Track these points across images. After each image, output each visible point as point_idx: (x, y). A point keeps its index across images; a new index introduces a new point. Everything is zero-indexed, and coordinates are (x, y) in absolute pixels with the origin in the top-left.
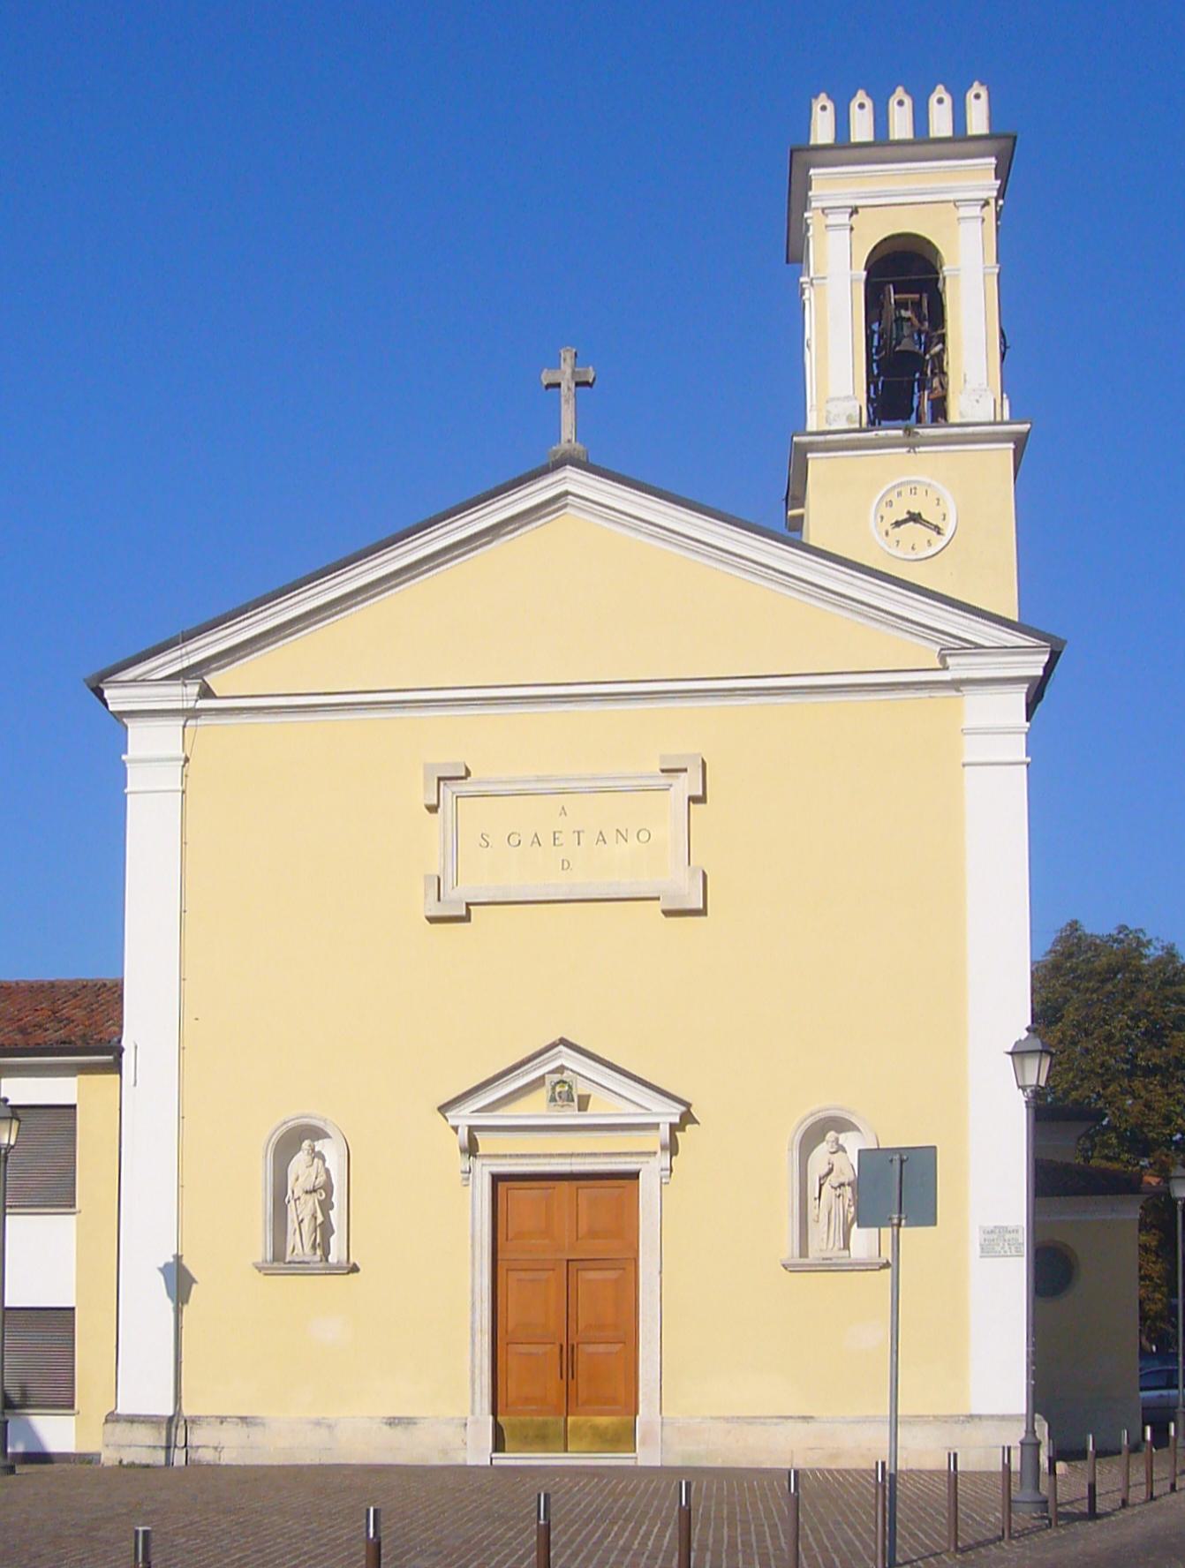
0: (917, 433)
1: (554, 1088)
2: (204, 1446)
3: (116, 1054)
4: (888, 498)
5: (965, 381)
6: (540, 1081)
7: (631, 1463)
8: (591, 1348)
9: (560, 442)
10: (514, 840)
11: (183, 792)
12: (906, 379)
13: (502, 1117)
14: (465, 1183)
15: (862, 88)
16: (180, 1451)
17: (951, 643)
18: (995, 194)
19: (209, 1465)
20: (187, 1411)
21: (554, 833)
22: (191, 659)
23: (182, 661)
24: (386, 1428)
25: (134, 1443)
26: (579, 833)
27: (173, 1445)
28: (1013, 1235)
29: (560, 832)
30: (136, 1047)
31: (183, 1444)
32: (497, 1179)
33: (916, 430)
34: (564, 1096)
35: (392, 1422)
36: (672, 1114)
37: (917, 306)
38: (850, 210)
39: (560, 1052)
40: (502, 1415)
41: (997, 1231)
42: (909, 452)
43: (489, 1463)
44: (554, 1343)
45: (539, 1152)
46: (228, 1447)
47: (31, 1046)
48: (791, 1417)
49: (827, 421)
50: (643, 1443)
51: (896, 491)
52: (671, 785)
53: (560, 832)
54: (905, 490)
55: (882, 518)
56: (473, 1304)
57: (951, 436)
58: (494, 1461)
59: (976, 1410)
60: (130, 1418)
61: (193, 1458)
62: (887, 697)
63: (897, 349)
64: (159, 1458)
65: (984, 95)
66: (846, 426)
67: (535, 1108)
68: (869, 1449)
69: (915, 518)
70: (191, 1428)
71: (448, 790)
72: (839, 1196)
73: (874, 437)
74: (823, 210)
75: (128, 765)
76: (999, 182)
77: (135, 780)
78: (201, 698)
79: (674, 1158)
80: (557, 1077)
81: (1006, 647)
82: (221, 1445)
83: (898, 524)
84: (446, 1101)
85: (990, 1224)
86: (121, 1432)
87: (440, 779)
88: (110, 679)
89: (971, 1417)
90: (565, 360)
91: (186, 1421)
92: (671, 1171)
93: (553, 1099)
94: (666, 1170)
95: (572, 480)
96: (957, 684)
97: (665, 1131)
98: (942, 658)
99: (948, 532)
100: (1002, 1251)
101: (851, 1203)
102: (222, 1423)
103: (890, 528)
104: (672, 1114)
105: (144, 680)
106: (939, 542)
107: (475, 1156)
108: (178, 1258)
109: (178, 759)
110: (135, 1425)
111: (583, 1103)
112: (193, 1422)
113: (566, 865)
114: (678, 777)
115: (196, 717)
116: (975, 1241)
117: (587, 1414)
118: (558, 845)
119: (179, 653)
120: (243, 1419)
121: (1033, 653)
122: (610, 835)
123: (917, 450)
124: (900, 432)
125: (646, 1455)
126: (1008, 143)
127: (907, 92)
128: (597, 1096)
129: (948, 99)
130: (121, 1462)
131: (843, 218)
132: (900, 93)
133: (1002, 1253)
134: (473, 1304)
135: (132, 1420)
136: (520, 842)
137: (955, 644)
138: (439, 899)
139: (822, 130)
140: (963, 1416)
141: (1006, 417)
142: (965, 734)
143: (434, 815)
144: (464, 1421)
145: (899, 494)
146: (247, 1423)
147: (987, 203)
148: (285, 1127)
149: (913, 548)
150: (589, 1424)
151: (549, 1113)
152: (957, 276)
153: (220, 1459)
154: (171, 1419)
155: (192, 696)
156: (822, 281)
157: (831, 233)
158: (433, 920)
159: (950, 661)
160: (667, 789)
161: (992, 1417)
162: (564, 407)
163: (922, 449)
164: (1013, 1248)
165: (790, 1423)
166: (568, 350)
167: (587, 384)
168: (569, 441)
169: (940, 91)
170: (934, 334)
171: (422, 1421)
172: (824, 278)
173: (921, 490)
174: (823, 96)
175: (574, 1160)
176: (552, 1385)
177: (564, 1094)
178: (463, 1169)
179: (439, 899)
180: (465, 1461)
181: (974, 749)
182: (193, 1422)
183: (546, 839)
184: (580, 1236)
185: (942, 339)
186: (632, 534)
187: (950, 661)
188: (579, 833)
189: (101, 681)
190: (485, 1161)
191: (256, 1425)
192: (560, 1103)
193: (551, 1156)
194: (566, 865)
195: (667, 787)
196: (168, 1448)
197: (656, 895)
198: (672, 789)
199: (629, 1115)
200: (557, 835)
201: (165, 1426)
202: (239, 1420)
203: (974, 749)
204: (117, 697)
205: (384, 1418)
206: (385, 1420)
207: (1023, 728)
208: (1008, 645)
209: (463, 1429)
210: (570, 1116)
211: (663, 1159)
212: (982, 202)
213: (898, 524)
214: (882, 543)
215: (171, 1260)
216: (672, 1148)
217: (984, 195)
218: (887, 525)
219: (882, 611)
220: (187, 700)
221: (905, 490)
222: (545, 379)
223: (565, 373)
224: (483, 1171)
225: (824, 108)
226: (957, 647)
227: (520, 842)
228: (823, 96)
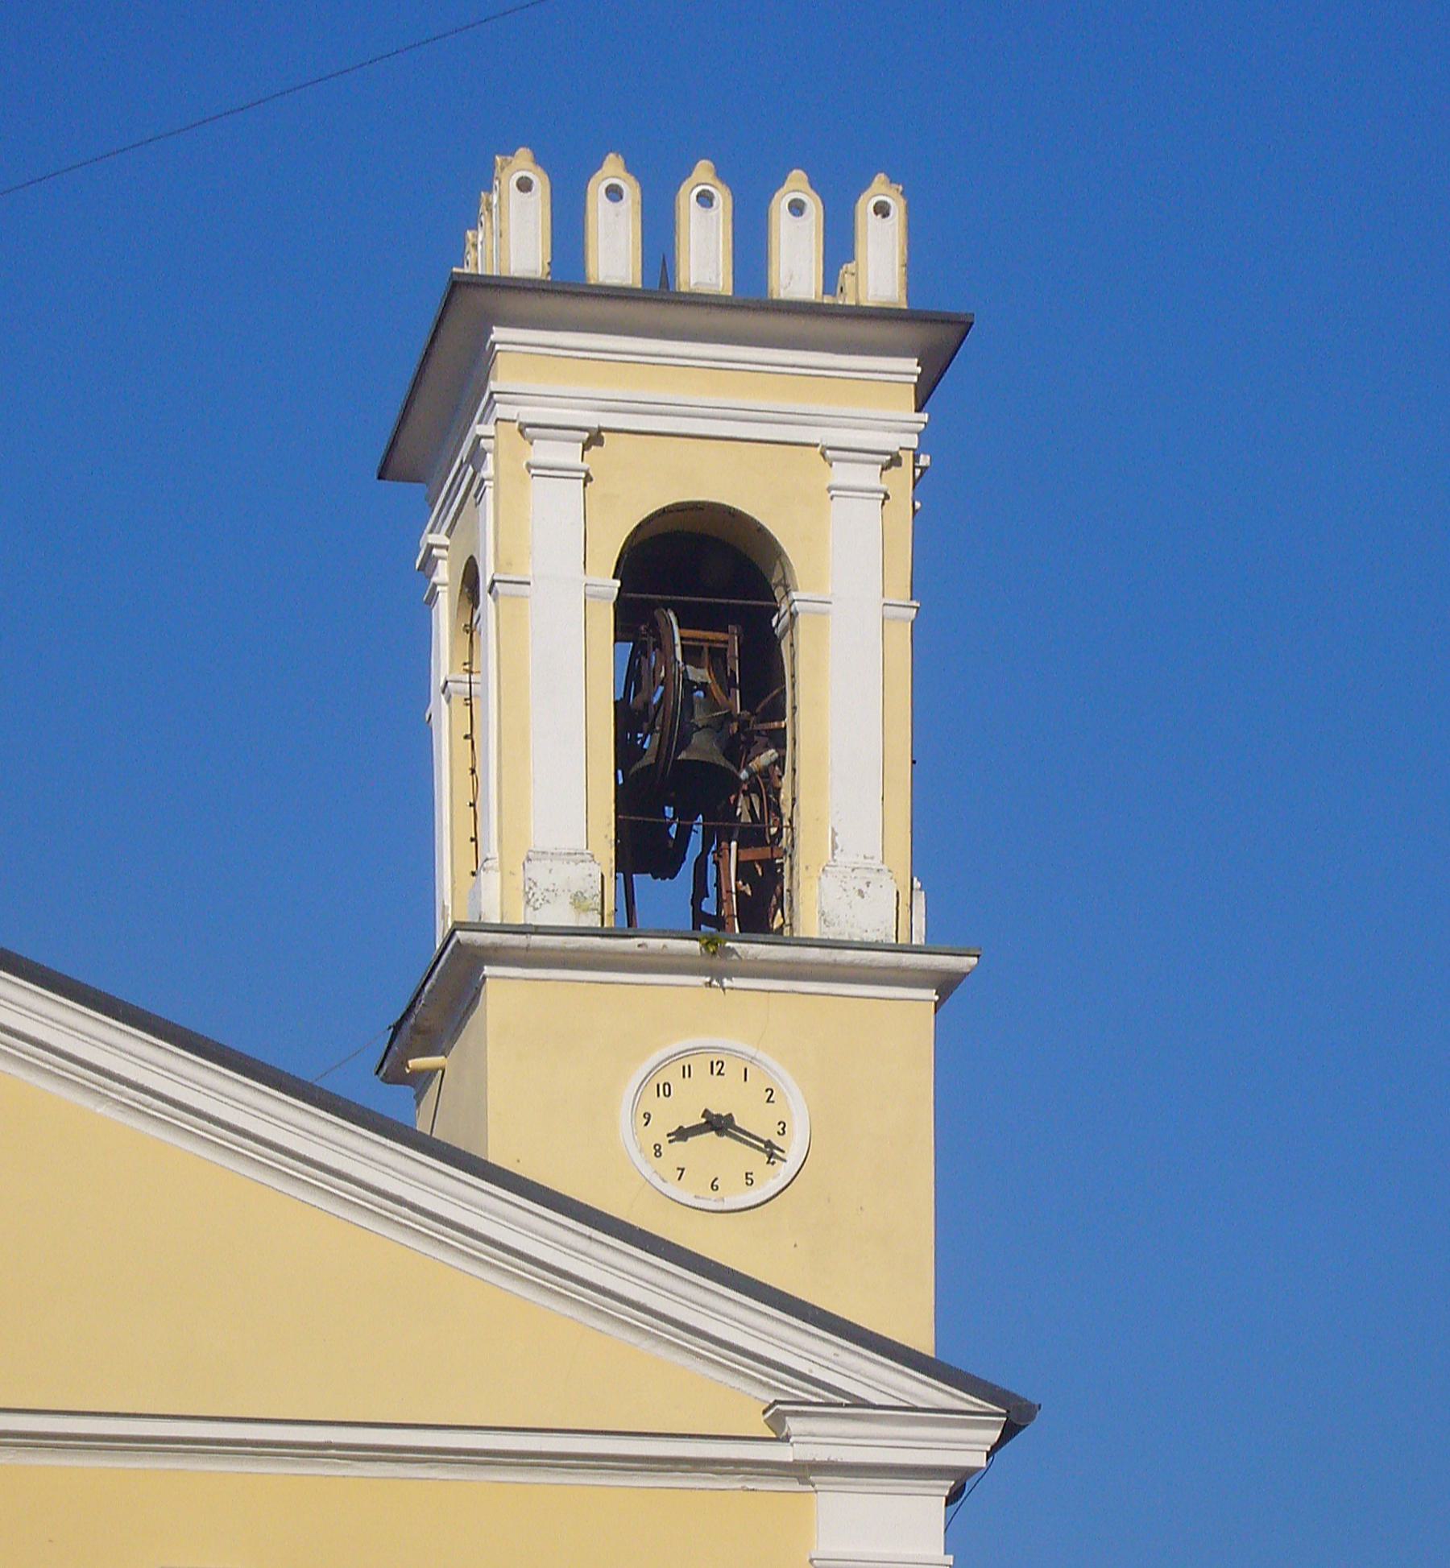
0: (732, 951)
5: (834, 847)
15: (618, 152)
18: (913, 441)
37: (718, 656)
44: (883, 862)
51: (679, 1065)
63: (683, 756)
65: (897, 207)
66: (569, 919)
69: (718, 1124)
83: (682, 1134)
98: (776, 1419)
99: (794, 1148)
103: (664, 1141)
106: (772, 1179)
127: (721, 174)
129: (814, 207)
131: (569, 454)
132: (703, 174)
137: (819, 1396)
141: (918, 940)
145: (687, 1072)
147: (895, 461)
152: (825, 613)
159: (793, 1425)
170: (760, 727)
173: (733, 1069)
174: (524, 156)
185: (778, 739)
186: (87, 1102)
187: (793, 1425)
208: (920, 1405)
213: (682, 1134)
214: (647, 1171)
217: (892, 442)
221: (700, 1065)
226: (815, 1399)
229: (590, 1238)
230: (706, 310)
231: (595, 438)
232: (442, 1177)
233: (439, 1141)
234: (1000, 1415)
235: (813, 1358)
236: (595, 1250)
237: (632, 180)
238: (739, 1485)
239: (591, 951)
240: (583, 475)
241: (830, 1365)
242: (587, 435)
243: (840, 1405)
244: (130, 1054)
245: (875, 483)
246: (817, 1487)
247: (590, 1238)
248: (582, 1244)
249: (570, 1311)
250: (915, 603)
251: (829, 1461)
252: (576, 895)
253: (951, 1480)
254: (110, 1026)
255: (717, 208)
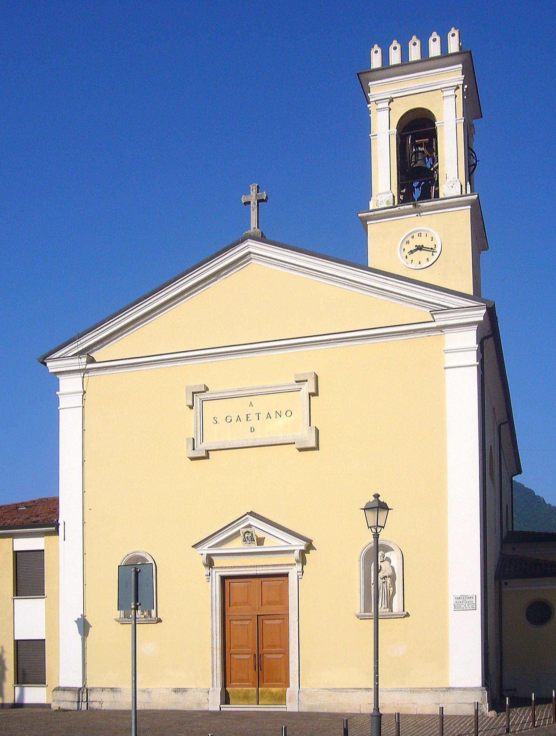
0: (420, 206)
1: (244, 535)
2: (95, 701)
3: (56, 526)
4: (407, 240)
5: (446, 178)
6: (237, 534)
7: (284, 710)
8: (268, 656)
9: (250, 229)
10: (228, 419)
11: (83, 407)
12: (410, 182)
13: (223, 549)
14: (208, 580)
15: (395, 39)
16: (84, 703)
17: (437, 308)
18: (462, 82)
19: (97, 710)
20: (89, 686)
21: (247, 415)
22: (79, 349)
23: (78, 348)
24: (173, 693)
25: (65, 700)
26: (258, 414)
27: (81, 700)
28: (471, 600)
29: (250, 414)
30: (64, 523)
31: (86, 700)
32: (223, 579)
33: (418, 204)
34: (250, 539)
35: (176, 690)
36: (301, 545)
38: (388, 100)
39: (248, 518)
40: (228, 687)
41: (462, 598)
42: (417, 216)
43: (219, 710)
45: (241, 565)
46: (105, 702)
47: (21, 524)
48: (361, 689)
49: (377, 205)
50: (290, 701)
52: (301, 388)
53: (250, 414)
54: (416, 235)
55: (404, 249)
56: (212, 636)
57: (437, 205)
58: (221, 708)
59: (451, 685)
60: (64, 689)
61: (90, 706)
62: (205, 361)
64: (75, 706)
67: (237, 545)
68: (398, 704)
69: (420, 248)
70: (89, 693)
71: (197, 398)
72: (384, 582)
73: (398, 210)
74: (375, 101)
75: (59, 397)
76: (464, 76)
77: (63, 402)
78: (88, 364)
79: (304, 566)
80: (245, 530)
81: (463, 308)
82: (102, 701)
83: (412, 252)
84: (196, 543)
85: (459, 595)
86: (60, 695)
87: (193, 393)
88: (48, 358)
89: (449, 688)
90: (252, 190)
91: (87, 690)
92: (303, 573)
93: (245, 541)
94: (300, 572)
95: (252, 246)
96: (440, 328)
97: (297, 553)
99: (438, 249)
100: (465, 608)
101: (391, 586)
102: (103, 691)
103: (408, 255)
104: (301, 545)
105: (64, 357)
107: (212, 568)
108: (83, 616)
109: (80, 392)
110: (66, 692)
111: (260, 542)
112: (91, 690)
113: (252, 430)
114: (304, 384)
115: (88, 373)
116: (451, 602)
117: (267, 686)
118: (249, 421)
119: (76, 344)
120: (112, 689)
121: (466, 311)
122: (273, 414)
123: (421, 214)
124: (411, 206)
125: (291, 707)
126: (466, 56)
128: (268, 538)
130: (59, 708)
133: (465, 609)
134: (212, 636)
135: (64, 689)
136: (231, 420)
137: (438, 308)
138: (194, 449)
139: (376, 61)
140: (445, 688)
142: (445, 353)
143: (192, 410)
144: (208, 690)
145: (413, 237)
146: (113, 691)
147: (458, 88)
148: (128, 557)
149: (420, 263)
150: (268, 691)
151: (244, 547)
153: (102, 707)
154: (80, 689)
155: (84, 362)
156: (443, 124)
157: (379, 112)
158: (192, 459)
160: (300, 391)
161: (459, 688)
162: (252, 212)
163: (424, 213)
164: (470, 606)
165: (360, 692)
166: (254, 185)
167: (263, 200)
168: (254, 228)
169: (435, 35)
171: (190, 690)
172: (376, 135)
173: (423, 235)
174: (376, 46)
175: (258, 569)
176: (252, 674)
177: (249, 538)
178: (206, 574)
179: (194, 449)
180: (208, 709)
181: (450, 360)
182: (91, 690)
183: (243, 418)
184: (263, 604)
188: (258, 414)
189: (45, 359)
190: (217, 570)
191: (116, 691)
192: (248, 542)
193: (247, 567)
194: (252, 430)
195: (300, 389)
196: (79, 702)
197: (293, 442)
198: (301, 390)
199: (283, 546)
200: (248, 416)
201: (77, 692)
202: (110, 690)
203: (450, 360)
204: (52, 366)
205: (173, 689)
206: (173, 690)
207: (476, 347)
209: (207, 694)
210: (254, 548)
211: (299, 567)
212: (455, 87)
213: (412, 252)
214: (404, 262)
215: (80, 617)
216: (303, 561)
218: (406, 253)
219: (402, 295)
220: (82, 365)
221: (416, 235)
222: (243, 201)
223: (252, 196)
224: (216, 575)
225: (395, 48)
227: (231, 420)
228: (376, 46)
229: (386, 279)
230: (411, 65)
231: (391, 100)
232: (350, 270)
233: (371, 268)
234: (484, 305)
235: (441, 300)
236: (388, 282)
237: (399, 44)
238: (427, 335)
239: (389, 212)
240: (388, 109)
241: (444, 300)
242: (388, 100)
243: (445, 310)
244: (324, 266)
245: (454, 93)
246: (445, 332)
247: (386, 279)
248: (385, 281)
249: (387, 299)
250: (464, 118)
251: (445, 325)
252: (387, 201)
253: (476, 325)
254: (274, 248)
255: (413, 41)
